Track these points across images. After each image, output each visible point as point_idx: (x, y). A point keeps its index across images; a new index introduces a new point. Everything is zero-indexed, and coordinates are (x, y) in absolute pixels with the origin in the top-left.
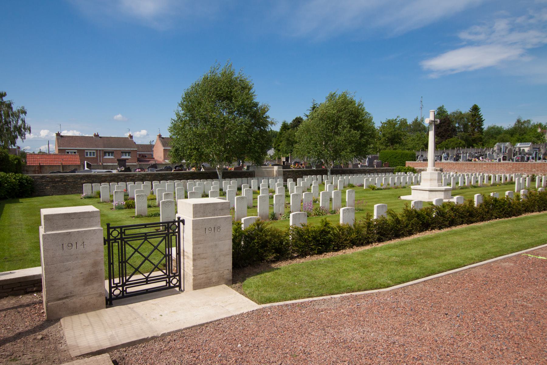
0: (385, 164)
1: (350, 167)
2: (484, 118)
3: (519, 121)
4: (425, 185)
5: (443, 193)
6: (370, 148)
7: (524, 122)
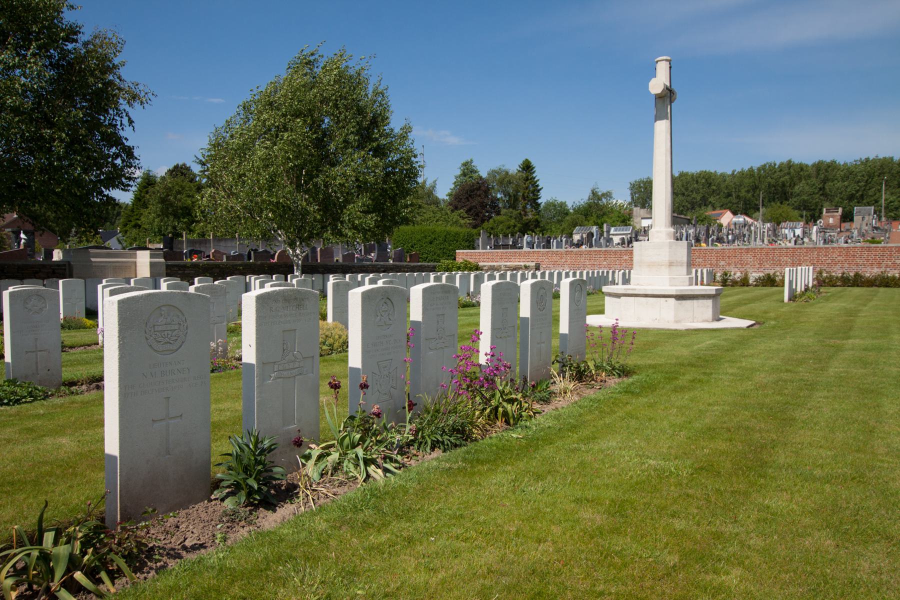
0: (411, 256)
1: (339, 257)
2: (541, 184)
3: (594, 193)
4: (641, 280)
5: (709, 303)
6: (407, 206)
7: (603, 195)
